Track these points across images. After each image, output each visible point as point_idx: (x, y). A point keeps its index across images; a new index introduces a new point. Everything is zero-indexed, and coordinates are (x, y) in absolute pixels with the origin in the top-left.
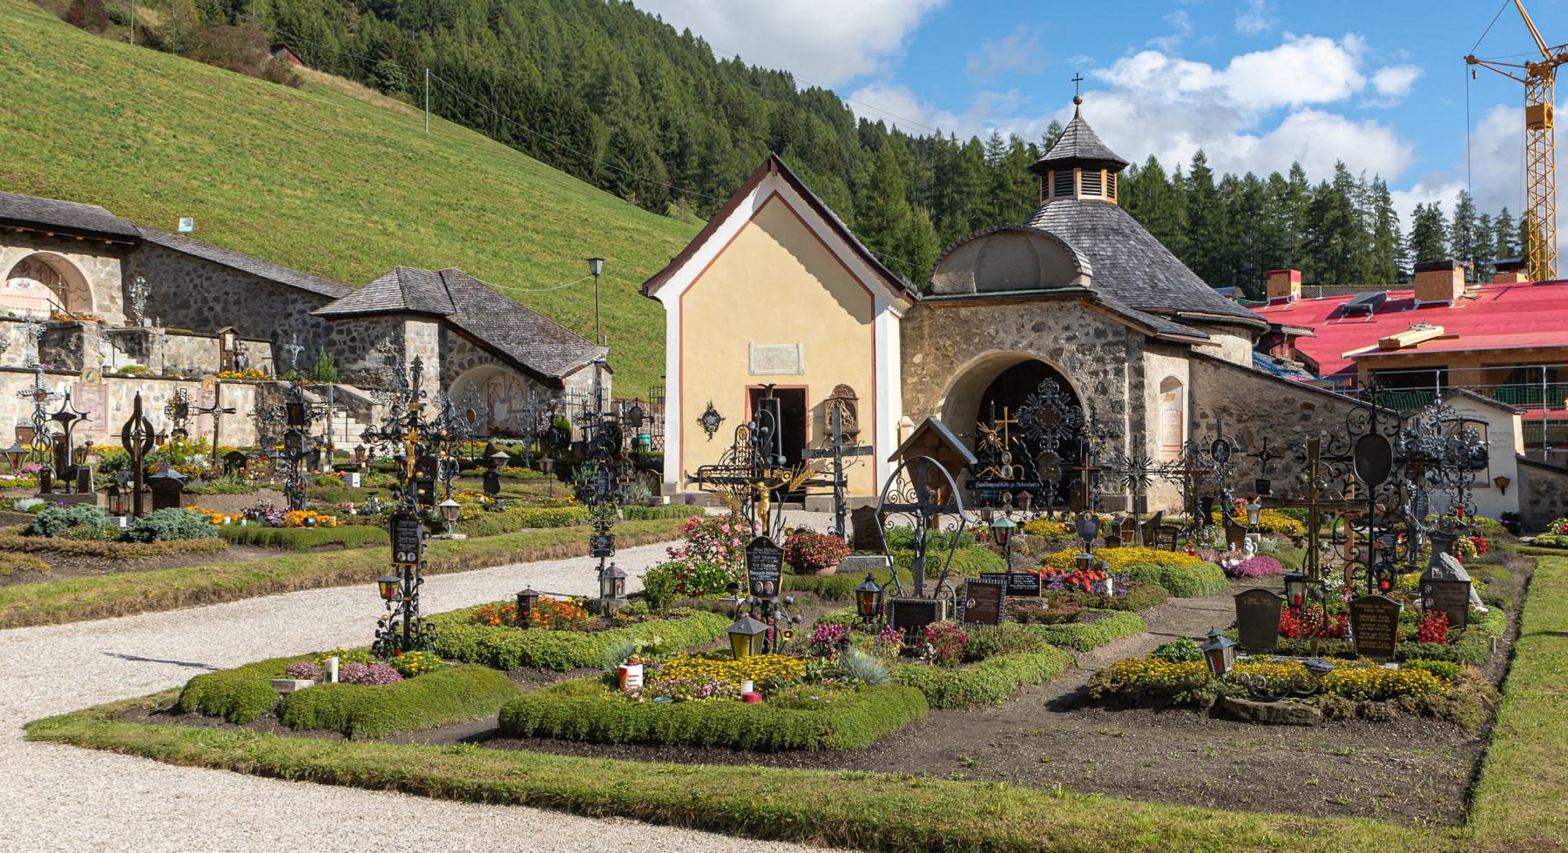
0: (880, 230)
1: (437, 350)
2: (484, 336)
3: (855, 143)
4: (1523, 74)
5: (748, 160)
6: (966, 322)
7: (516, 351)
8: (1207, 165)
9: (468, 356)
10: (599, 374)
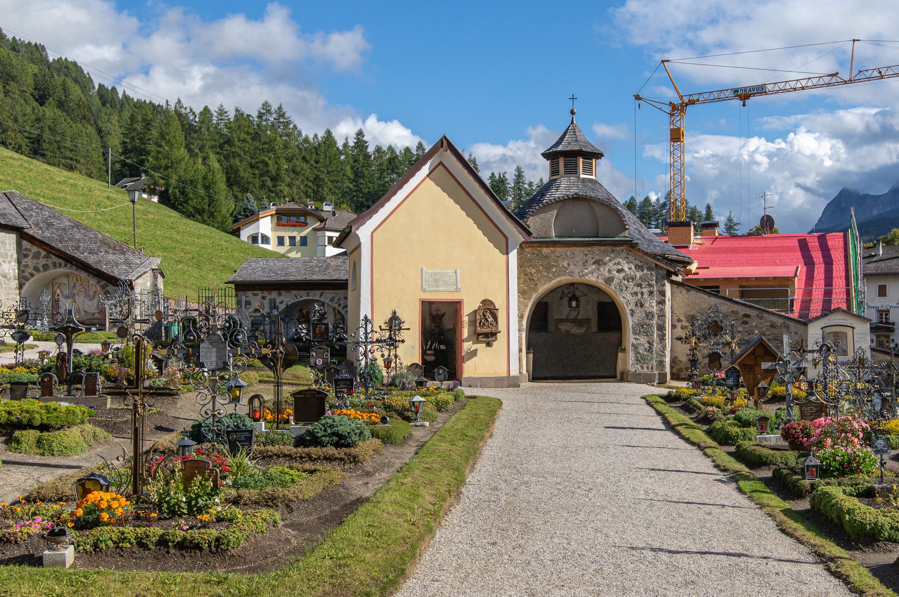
0: (167, 168)
1: (15, 256)
2: (60, 246)
3: (97, 101)
4: (668, 109)
5: (18, 108)
6: (546, 257)
7: (92, 260)
8: (365, 139)
9: (42, 261)
10: (155, 278)
